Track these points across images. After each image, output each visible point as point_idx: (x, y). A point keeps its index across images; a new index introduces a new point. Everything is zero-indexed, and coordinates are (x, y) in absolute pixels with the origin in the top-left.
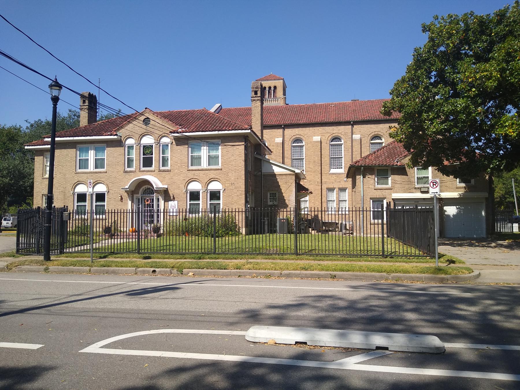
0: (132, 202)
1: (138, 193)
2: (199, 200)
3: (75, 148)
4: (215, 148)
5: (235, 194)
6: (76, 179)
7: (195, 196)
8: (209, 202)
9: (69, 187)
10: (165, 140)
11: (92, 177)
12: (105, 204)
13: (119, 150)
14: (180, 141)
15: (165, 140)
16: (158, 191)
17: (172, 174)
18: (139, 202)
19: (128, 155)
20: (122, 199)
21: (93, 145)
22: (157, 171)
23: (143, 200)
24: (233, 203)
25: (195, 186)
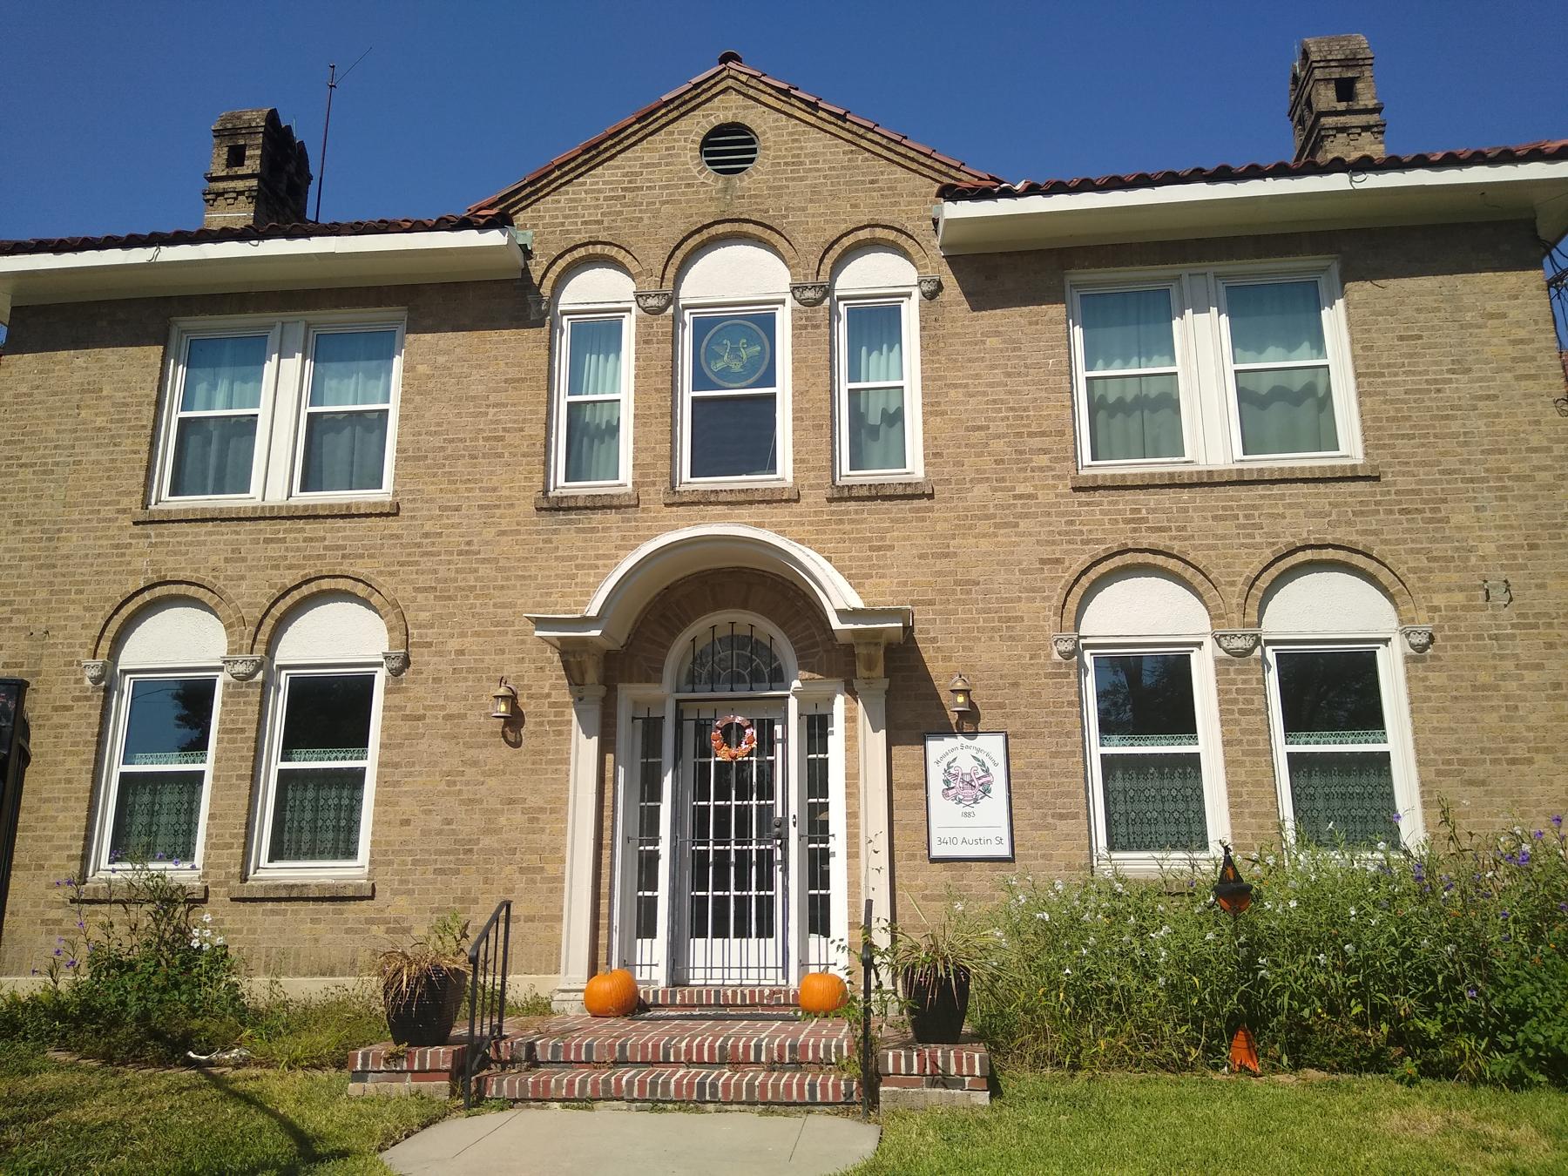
0: (606, 746)
1: (652, 674)
2: (359, 740)
3: (161, 338)
4: (248, 369)
5: (1530, 677)
6: (145, 559)
7: (1148, 693)
8: (275, 764)
9: (77, 628)
10: (871, 275)
11: (274, 550)
12: (208, 767)
13: (505, 348)
14: (995, 272)
15: (871, 275)
16: (838, 658)
17: (940, 516)
18: (651, 745)
19: (854, 375)
20: (514, 720)
21: (297, 322)
22: (814, 499)
23: (689, 727)
24: (1520, 751)
25: (1140, 613)
